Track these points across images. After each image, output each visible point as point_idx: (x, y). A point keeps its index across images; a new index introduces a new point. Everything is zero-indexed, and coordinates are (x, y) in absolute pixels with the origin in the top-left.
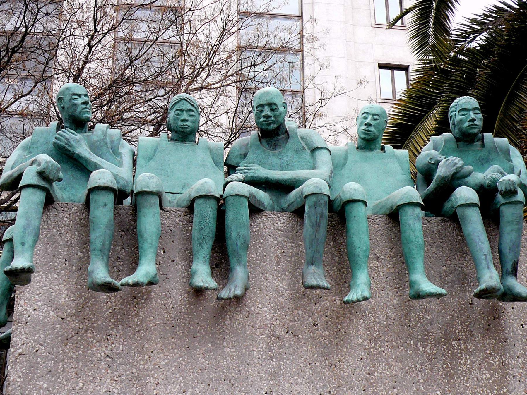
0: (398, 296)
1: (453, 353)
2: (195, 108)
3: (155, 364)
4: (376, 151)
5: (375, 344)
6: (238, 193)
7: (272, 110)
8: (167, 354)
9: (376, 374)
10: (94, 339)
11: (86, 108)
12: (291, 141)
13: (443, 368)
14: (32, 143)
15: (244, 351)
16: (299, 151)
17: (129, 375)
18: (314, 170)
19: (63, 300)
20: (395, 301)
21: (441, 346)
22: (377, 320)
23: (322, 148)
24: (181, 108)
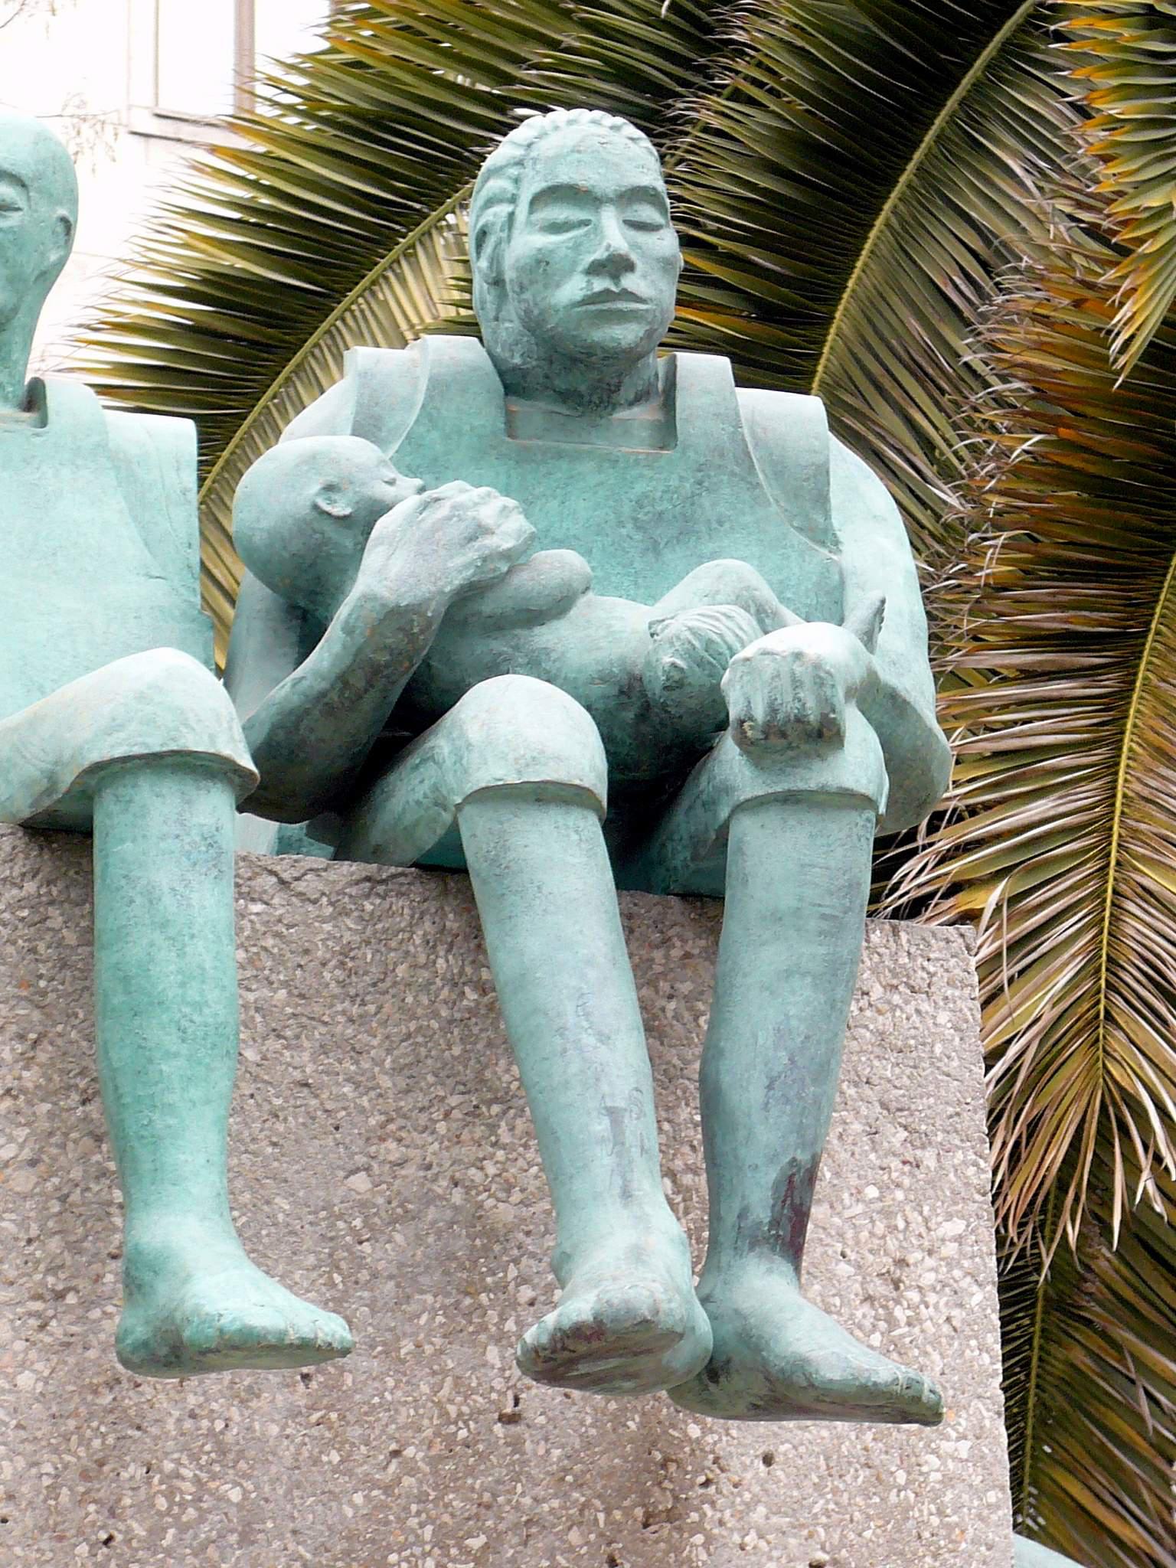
0: (47, 1349)
20: (25, 1380)
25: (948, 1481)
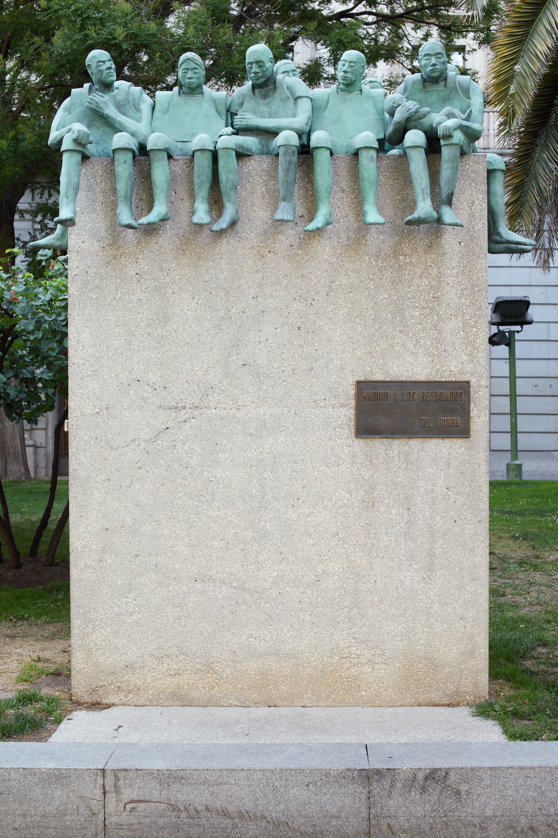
0: (358, 222)
1: (399, 265)
2: (199, 66)
3: (171, 279)
4: (354, 93)
5: (338, 260)
6: (226, 147)
7: (260, 67)
8: (180, 271)
9: (337, 282)
10: (127, 261)
11: (110, 73)
12: (278, 91)
13: (390, 277)
14: (71, 105)
15: (236, 267)
16: (284, 100)
17: (153, 287)
18: (295, 117)
19: (102, 234)
20: (355, 225)
21: (390, 260)
22: (340, 241)
23: (303, 97)
24: (187, 67)
25: (479, 230)
